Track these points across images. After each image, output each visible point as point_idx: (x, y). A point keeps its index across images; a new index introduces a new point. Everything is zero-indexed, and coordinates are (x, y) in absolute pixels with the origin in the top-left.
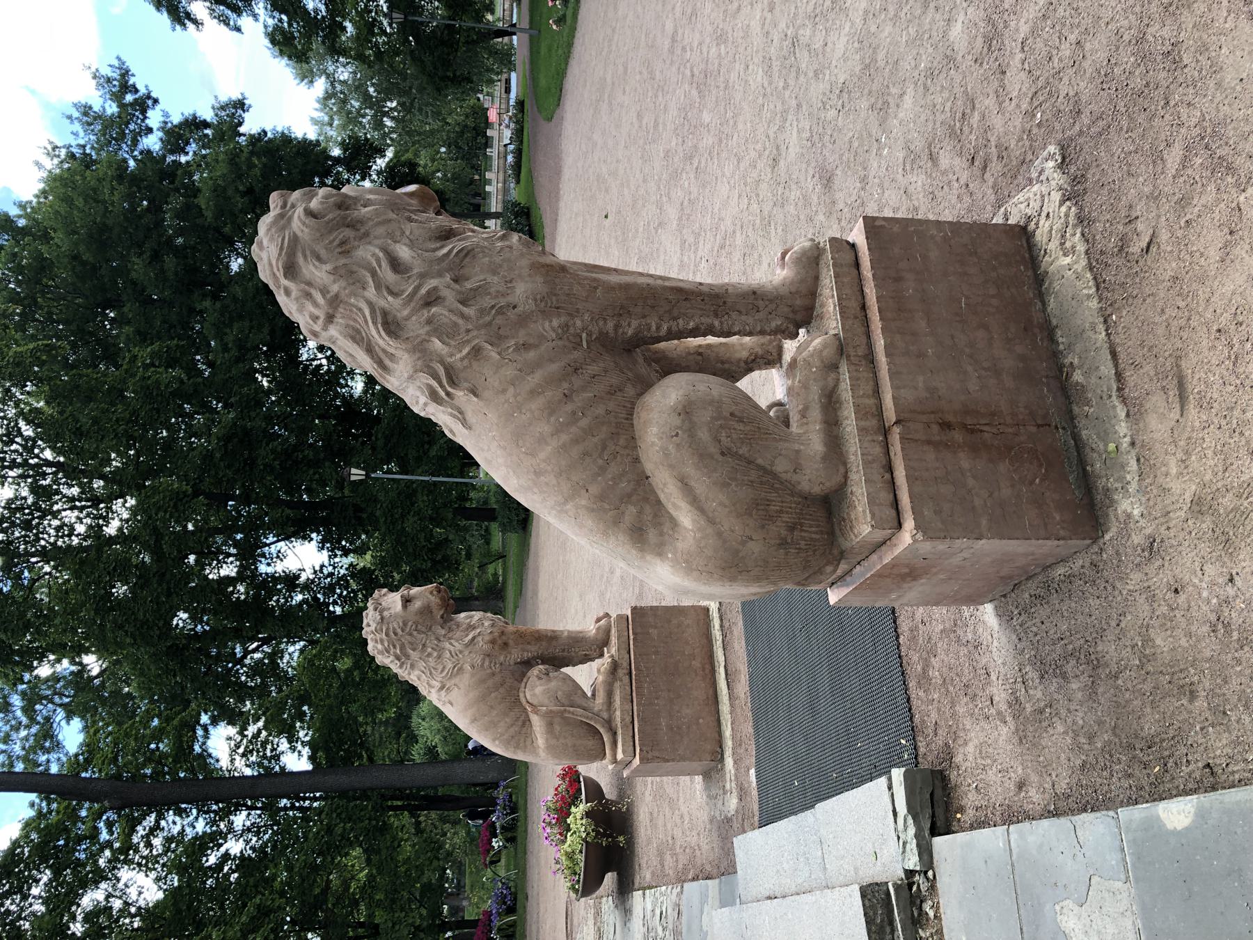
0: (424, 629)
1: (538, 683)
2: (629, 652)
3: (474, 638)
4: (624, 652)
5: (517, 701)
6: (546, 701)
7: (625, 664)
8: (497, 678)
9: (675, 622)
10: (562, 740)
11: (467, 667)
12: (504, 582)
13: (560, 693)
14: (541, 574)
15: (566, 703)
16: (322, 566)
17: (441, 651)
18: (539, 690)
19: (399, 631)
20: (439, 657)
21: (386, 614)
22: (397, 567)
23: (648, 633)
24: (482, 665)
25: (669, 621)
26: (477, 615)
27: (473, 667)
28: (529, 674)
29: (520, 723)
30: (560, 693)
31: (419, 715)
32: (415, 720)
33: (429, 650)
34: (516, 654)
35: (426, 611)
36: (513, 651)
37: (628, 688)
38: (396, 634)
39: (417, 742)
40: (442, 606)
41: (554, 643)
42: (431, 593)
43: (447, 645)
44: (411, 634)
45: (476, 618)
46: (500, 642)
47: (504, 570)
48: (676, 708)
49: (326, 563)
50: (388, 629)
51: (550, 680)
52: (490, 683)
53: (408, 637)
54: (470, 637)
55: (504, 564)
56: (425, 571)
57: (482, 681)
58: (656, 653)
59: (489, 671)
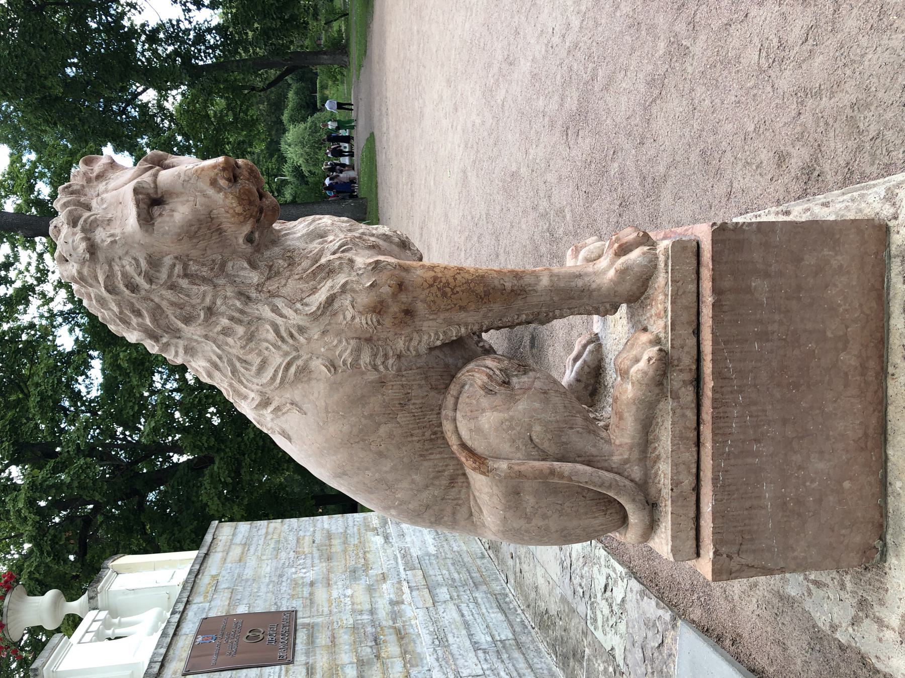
0: (205, 272)
1: (485, 402)
2: (697, 332)
3: (331, 300)
4: (686, 332)
5: (437, 438)
6: (506, 448)
7: (687, 361)
8: (391, 393)
9: (810, 260)
10: (537, 521)
11: (318, 366)
12: (348, 40)
13: (537, 428)
14: (389, 42)
15: (552, 449)
16: (178, 21)
17: (252, 324)
18: (489, 419)
19: (140, 281)
20: (250, 337)
21: (101, 235)
22: (250, 25)
23: (749, 290)
24: (355, 365)
25: (798, 260)
26: (326, 220)
27: (332, 366)
28: (463, 375)
29: (445, 482)
30: (537, 428)
31: (286, 142)
32: (283, 146)
33: (225, 322)
34: (432, 331)
35: (205, 227)
36: (426, 325)
37: (691, 415)
38: (133, 288)
39: (286, 162)
40: (244, 218)
41: (519, 303)
42: (214, 183)
43: (266, 312)
44: (173, 287)
45: (334, 241)
46: (394, 308)
47: (347, 26)
48: (797, 458)
49: (182, 18)
50: (110, 277)
51: (512, 398)
52: (375, 403)
53: (168, 294)
54: (321, 296)
55: (347, 21)
56: (274, 29)
57: (357, 401)
58: (764, 337)
59: (372, 376)
